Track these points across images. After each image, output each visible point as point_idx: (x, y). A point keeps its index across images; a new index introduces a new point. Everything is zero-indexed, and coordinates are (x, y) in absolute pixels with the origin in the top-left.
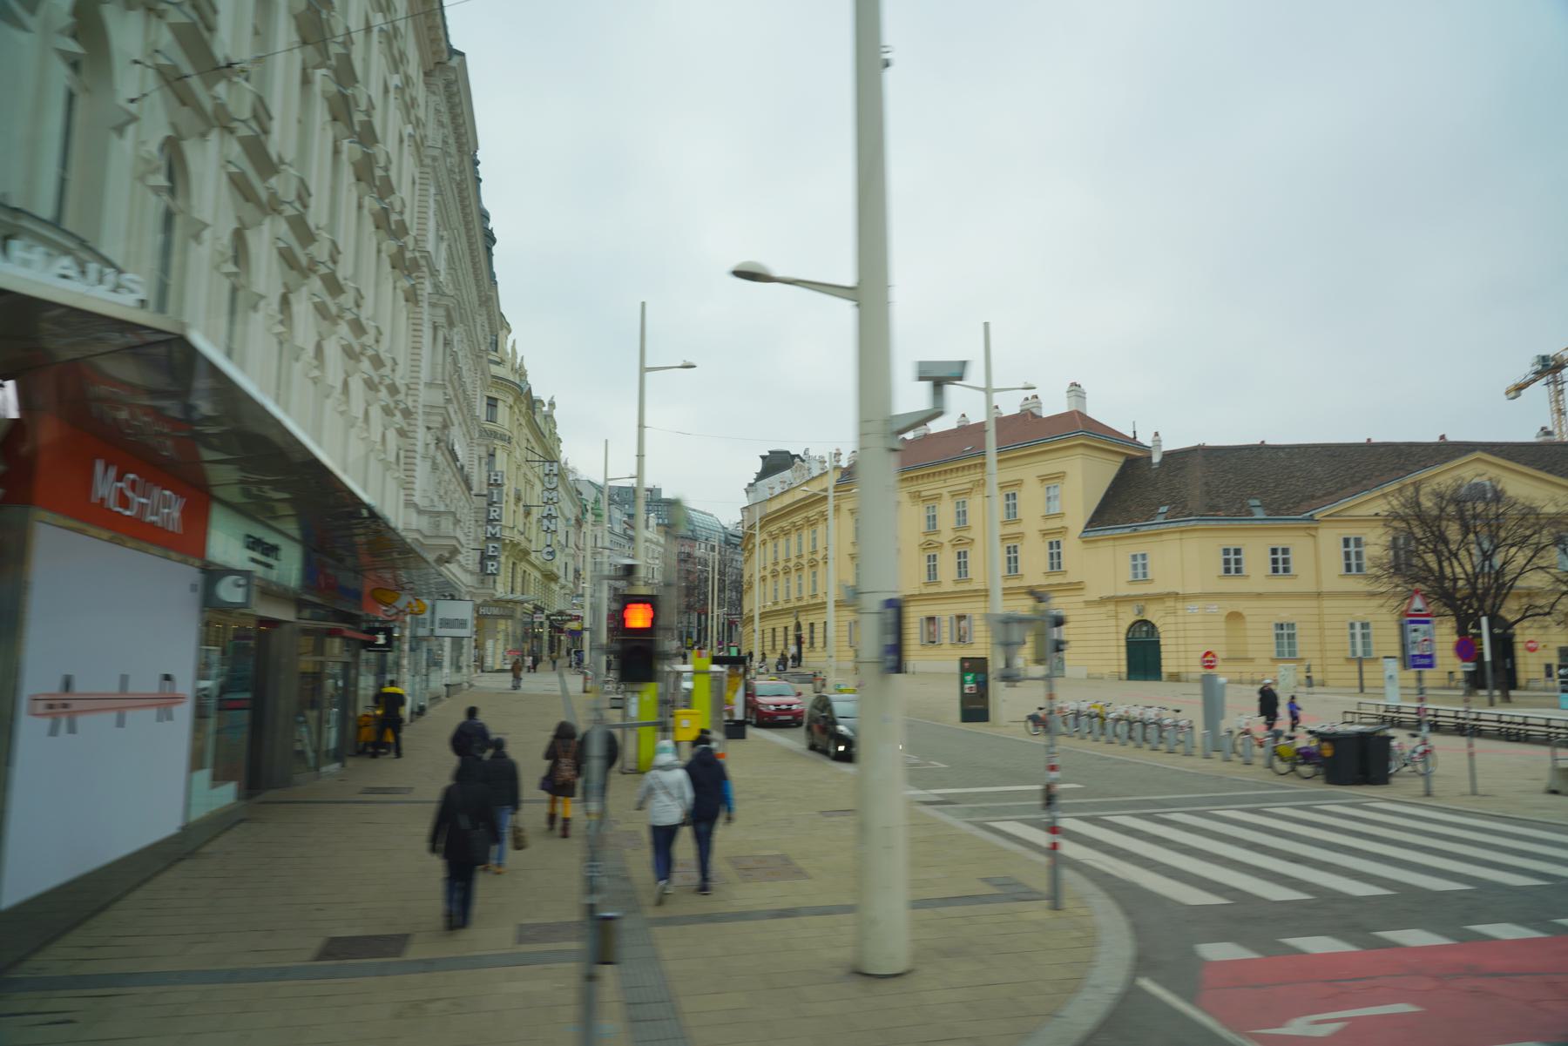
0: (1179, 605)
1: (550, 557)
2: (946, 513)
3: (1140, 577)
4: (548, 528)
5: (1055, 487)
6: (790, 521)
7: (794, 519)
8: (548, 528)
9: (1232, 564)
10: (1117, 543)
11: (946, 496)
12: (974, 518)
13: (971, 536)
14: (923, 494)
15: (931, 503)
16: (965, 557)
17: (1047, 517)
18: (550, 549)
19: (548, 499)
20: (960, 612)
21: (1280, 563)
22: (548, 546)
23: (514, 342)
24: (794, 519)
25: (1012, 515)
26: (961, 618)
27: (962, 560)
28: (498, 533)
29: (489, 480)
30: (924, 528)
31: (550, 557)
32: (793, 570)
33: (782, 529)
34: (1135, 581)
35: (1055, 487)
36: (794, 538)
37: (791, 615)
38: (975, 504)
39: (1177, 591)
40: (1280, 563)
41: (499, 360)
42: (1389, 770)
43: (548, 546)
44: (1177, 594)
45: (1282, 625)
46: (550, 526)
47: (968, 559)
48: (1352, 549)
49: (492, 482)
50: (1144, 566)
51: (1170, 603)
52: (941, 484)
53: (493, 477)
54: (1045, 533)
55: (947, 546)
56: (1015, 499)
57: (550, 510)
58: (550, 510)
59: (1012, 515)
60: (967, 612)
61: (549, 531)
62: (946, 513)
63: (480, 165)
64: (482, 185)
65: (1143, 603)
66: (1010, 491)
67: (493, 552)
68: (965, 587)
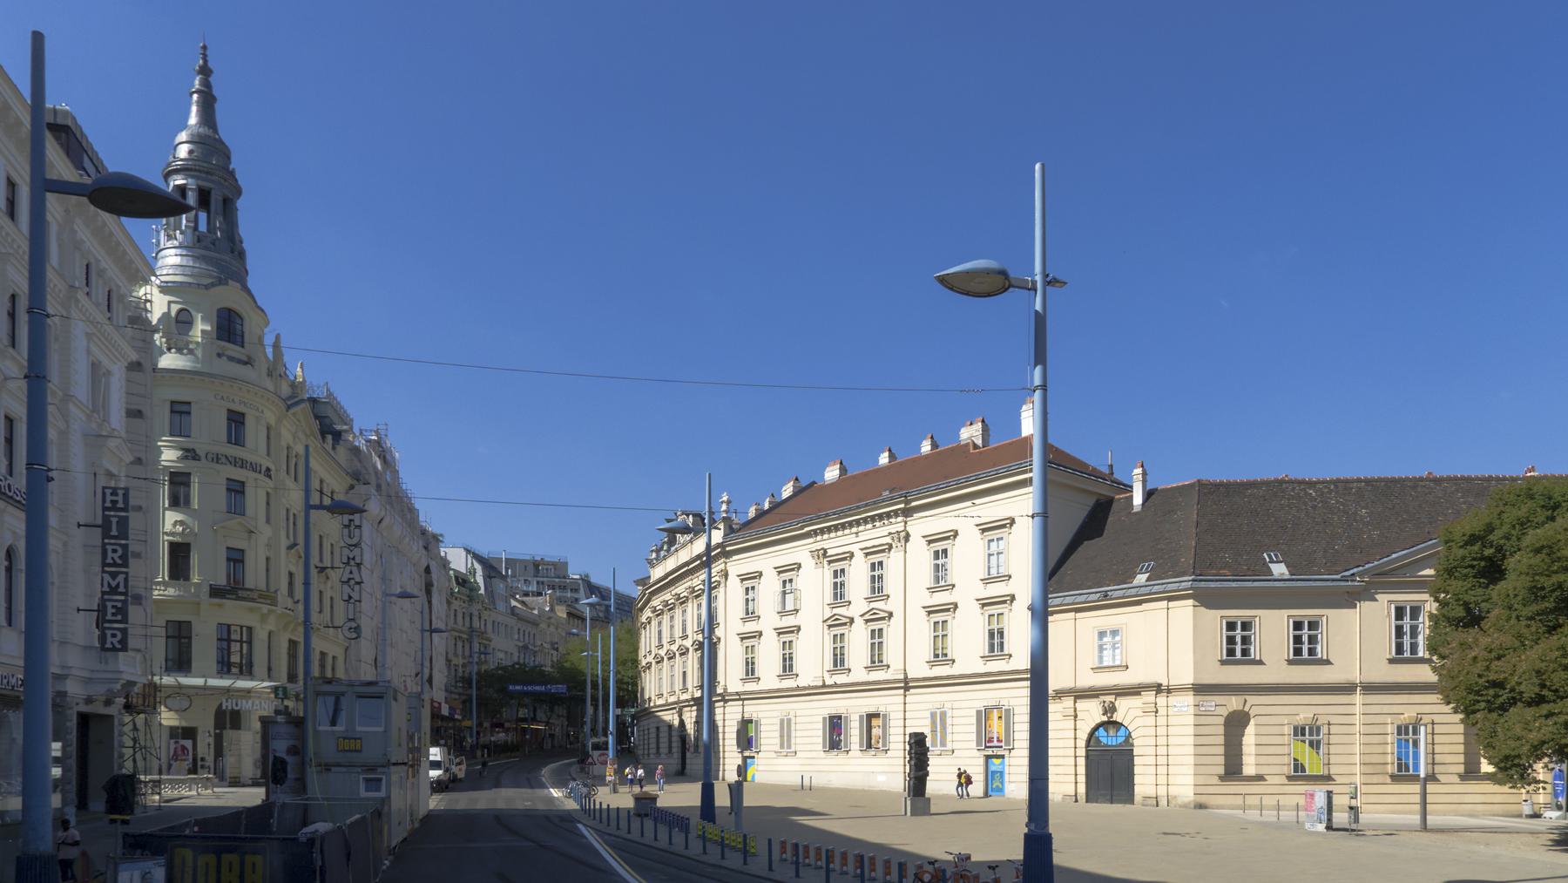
0: (1162, 700)
1: (354, 635)
2: (858, 576)
3: (1407, 654)
4: (350, 597)
5: (998, 539)
6: (673, 593)
7: (678, 590)
8: (350, 597)
9: (1238, 647)
10: (1079, 615)
11: (859, 555)
12: (892, 584)
13: (888, 608)
14: (830, 552)
15: (838, 566)
16: (880, 636)
17: (987, 581)
18: (354, 625)
19: (349, 558)
20: (872, 710)
21: (1304, 647)
22: (350, 620)
23: (278, 337)
24: (678, 590)
25: (940, 577)
26: (871, 716)
27: (877, 641)
28: (122, 585)
29: (104, 501)
30: (829, 598)
31: (354, 635)
32: (677, 655)
33: (666, 603)
34: (1230, 657)
35: (998, 539)
36: (678, 612)
37: (674, 711)
38: (893, 561)
39: (1159, 682)
40: (1304, 647)
41: (245, 359)
42: (151, 322)
43: (350, 620)
44: (1160, 685)
45: (1303, 729)
46: (350, 590)
47: (884, 640)
48: (1238, 633)
49: (108, 504)
50: (1245, 640)
51: (1149, 697)
52: (852, 539)
53: (109, 498)
54: (985, 603)
55: (859, 622)
56: (946, 557)
57: (351, 573)
58: (351, 573)
59: (940, 577)
60: (882, 710)
61: (352, 601)
62: (858, 576)
63: (213, 75)
64: (217, 106)
65: (1111, 698)
66: (939, 546)
67: (113, 614)
68: (841, 679)
